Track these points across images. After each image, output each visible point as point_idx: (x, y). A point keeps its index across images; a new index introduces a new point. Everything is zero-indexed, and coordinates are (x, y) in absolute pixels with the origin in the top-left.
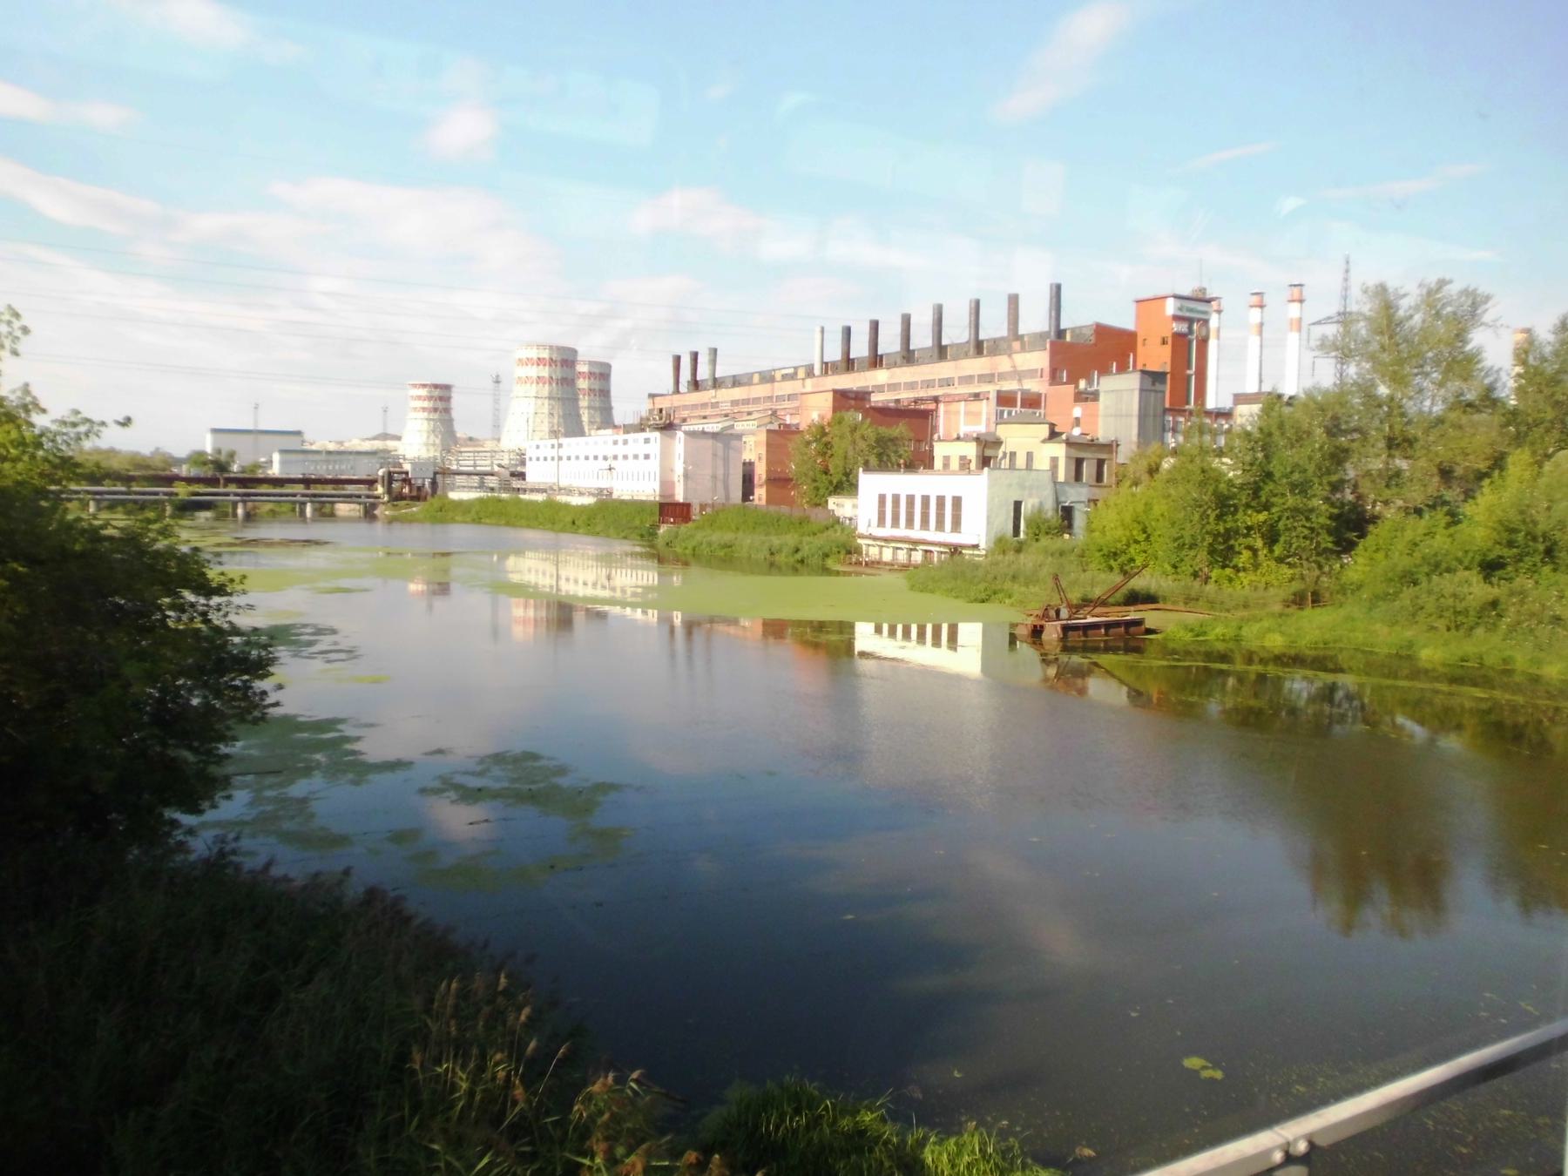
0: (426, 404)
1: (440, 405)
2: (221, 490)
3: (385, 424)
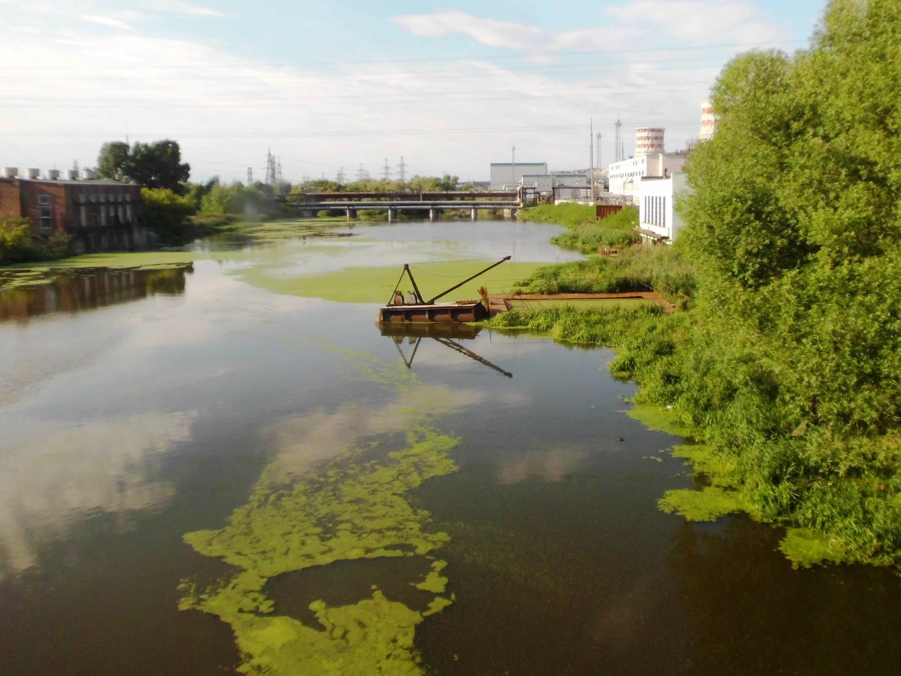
0: (647, 142)
1: (656, 142)
2: (421, 202)
3: (513, 158)
